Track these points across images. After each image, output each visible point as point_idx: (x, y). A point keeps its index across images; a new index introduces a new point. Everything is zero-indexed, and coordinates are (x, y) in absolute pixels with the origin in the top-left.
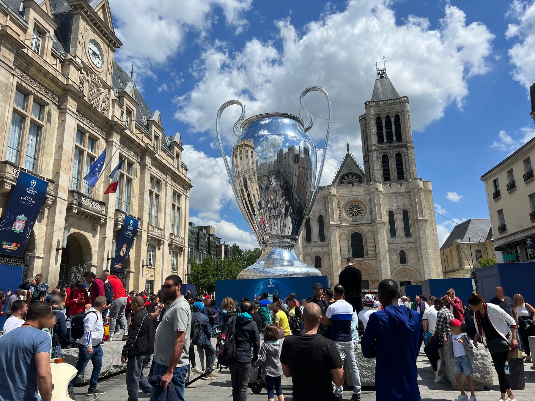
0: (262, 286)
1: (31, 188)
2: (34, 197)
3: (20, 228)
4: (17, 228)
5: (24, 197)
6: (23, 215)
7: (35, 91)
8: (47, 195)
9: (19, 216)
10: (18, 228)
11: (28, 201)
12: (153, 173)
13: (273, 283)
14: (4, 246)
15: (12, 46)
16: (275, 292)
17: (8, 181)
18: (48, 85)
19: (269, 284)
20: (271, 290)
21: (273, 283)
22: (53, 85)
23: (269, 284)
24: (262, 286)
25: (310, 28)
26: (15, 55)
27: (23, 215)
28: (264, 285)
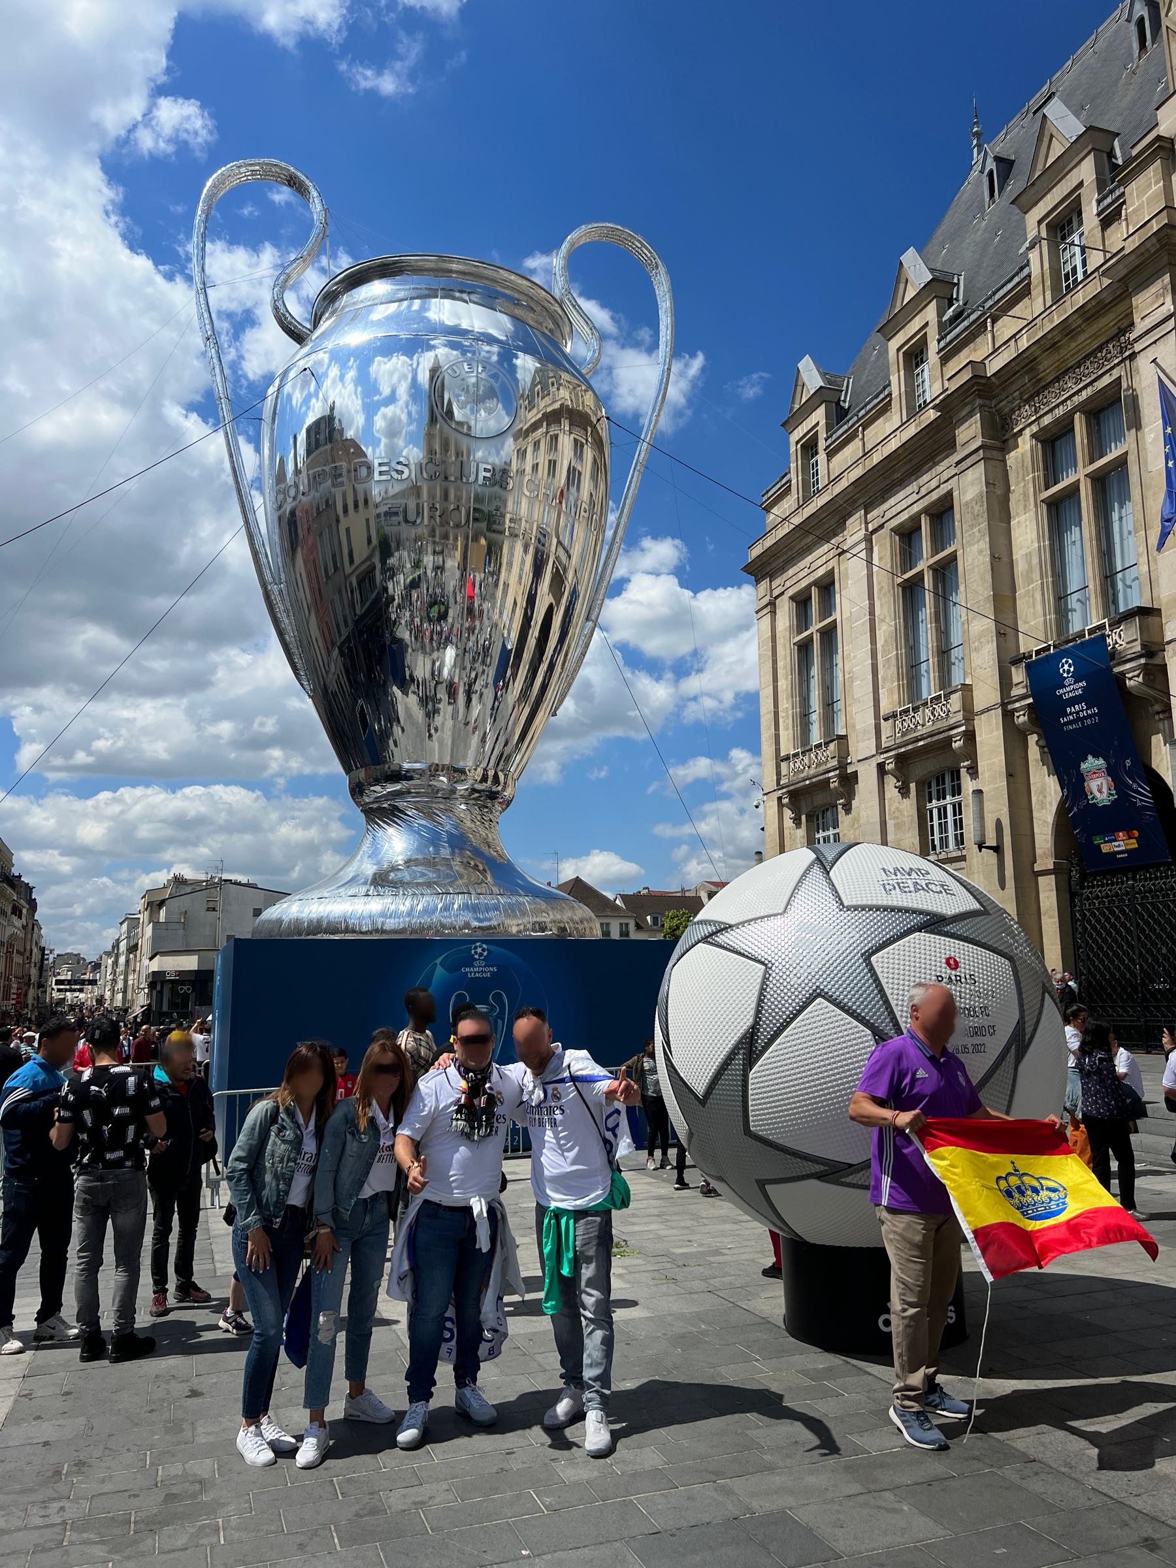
0: (440, 972)
1: (1066, 682)
2: (1086, 697)
3: (1105, 790)
4: (1098, 794)
5: (1066, 715)
6: (1090, 758)
7: (1075, 398)
8: (1116, 670)
9: (1083, 766)
10: (1100, 791)
11: (1079, 719)
12: (836, 571)
13: (489, 961)
14: (1105, 848)
15: (966, 405)
16: (498, 998)
17: (1017, 705)
18: (1095, 336)
19: (470, 961)
20: (480, 990)
21: (489, 961)
22: (1104, 321)
23: (470, 961)
24: (440, 972)
25: (295, 27)
26: (1130, 296)
27: (1090, 758)
28: (452, 967)
